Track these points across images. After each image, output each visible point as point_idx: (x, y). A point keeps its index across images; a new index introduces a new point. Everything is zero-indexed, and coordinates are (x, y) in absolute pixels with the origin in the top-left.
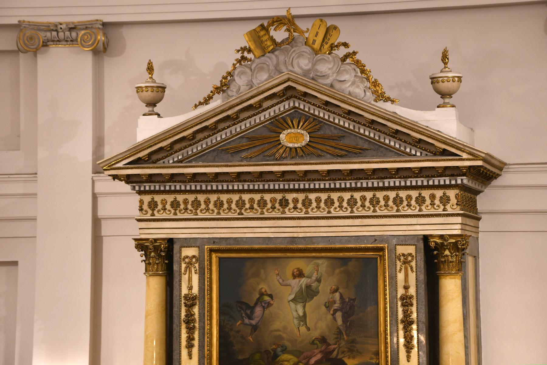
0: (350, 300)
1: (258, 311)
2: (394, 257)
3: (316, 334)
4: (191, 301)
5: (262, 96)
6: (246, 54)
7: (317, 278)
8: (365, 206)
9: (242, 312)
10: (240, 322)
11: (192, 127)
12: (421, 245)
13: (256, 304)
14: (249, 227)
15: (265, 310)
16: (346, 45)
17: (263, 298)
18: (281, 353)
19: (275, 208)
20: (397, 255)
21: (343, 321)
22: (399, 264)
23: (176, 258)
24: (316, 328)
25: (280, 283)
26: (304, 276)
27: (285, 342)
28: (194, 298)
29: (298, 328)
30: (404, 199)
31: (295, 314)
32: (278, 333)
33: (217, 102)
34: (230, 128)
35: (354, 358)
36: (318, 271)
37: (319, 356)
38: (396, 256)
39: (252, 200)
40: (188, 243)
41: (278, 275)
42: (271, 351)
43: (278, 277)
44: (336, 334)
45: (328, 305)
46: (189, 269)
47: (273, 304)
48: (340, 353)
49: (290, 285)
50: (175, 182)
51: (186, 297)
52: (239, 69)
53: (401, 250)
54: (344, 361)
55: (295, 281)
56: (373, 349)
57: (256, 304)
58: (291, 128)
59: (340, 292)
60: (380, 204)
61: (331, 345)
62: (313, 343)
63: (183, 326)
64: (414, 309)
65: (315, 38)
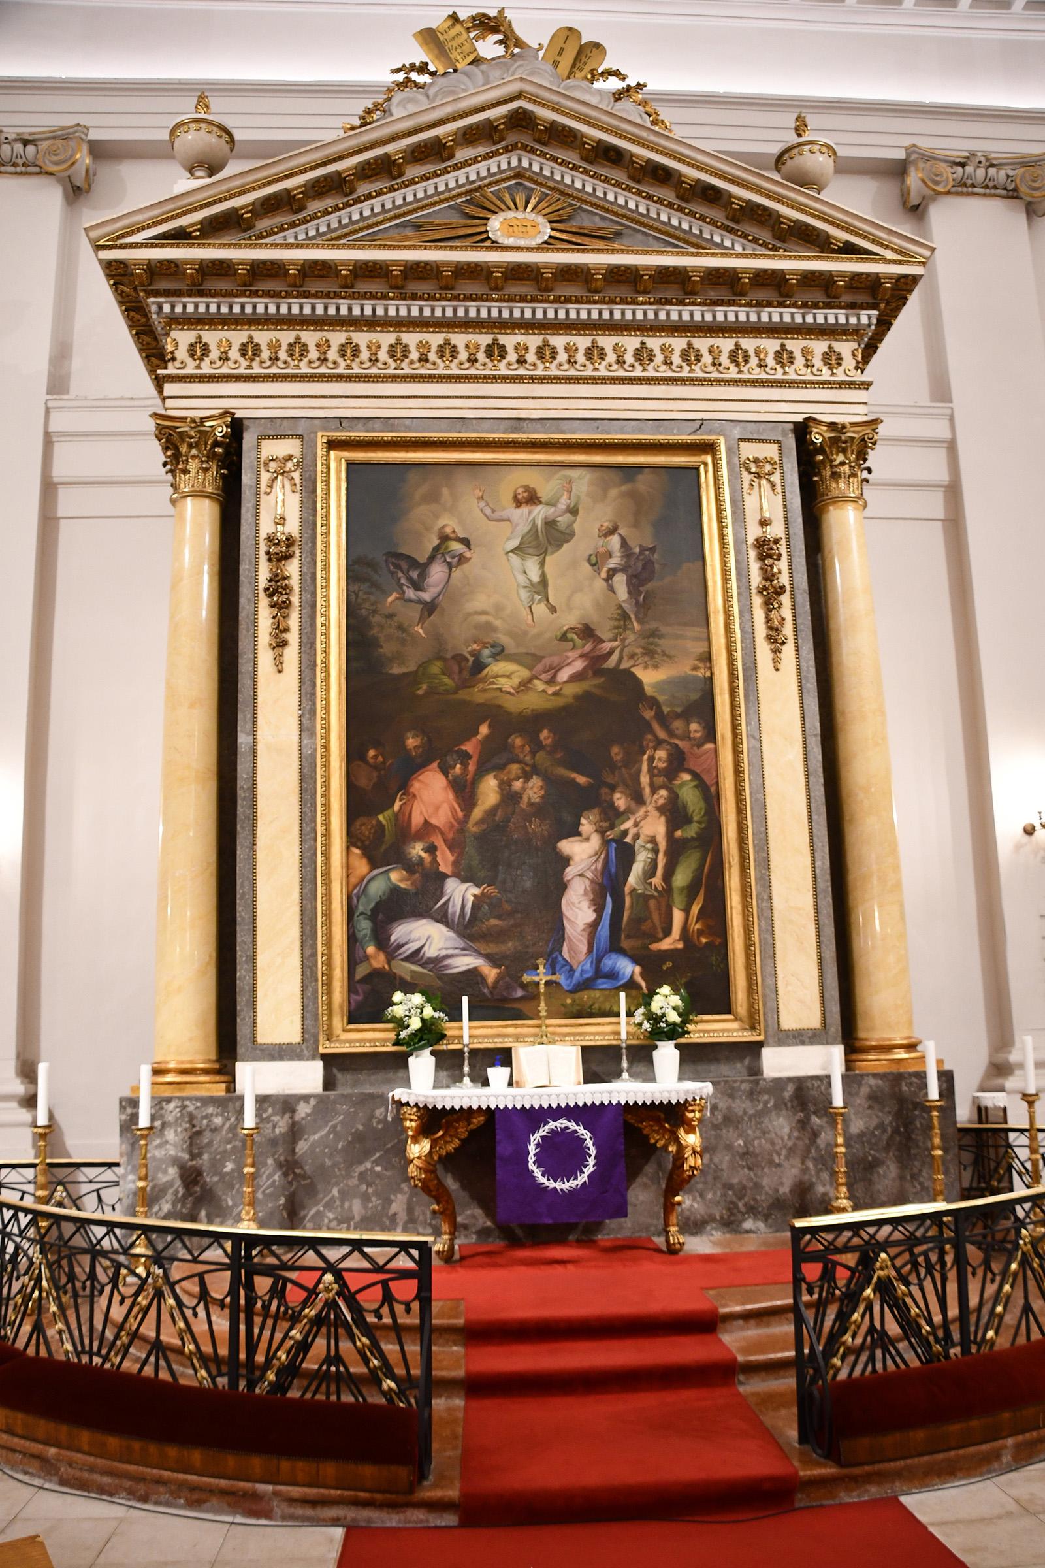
0: (643, 549)
1: (437, 572)
3: (570, 619)
4: (281, 552)
6: (414, 76)
7: (568, 506)
9: (400, 574)
10: (394, 595)
11: (305, 171)
12: (791, 442)
13: (432, 558)
16: (616, 74)
17: (447, 547)
18: (490, 659)
20: (742, 460)
21: (629, 592)
24: (569, 608)
25: (485, 515)
26: (541, 503)
27: (499, 635)
28: (290, 541)
31: (521, 579)
32: (483, 618)
34: (382, 198)
35: (656, 667)
36: (570, 492)
37: (579, 665)
39: (424, 346)
40: (276, 429)
41: (482, 498)
42: (468, 656)
43: (482, 504)
44: (616, 619)
45: (596, 561)
48: (625, 658)
50: (255, 294)
53: (749, 451)
54: (634, 675)
55: (519, 511)
56: (699, 648)
57: (432, 558)
58: (510, 209)
60: (703, 360)
62: (564, 638)
63: (264, 602)
64: (783, 565)
65: (558, 59)
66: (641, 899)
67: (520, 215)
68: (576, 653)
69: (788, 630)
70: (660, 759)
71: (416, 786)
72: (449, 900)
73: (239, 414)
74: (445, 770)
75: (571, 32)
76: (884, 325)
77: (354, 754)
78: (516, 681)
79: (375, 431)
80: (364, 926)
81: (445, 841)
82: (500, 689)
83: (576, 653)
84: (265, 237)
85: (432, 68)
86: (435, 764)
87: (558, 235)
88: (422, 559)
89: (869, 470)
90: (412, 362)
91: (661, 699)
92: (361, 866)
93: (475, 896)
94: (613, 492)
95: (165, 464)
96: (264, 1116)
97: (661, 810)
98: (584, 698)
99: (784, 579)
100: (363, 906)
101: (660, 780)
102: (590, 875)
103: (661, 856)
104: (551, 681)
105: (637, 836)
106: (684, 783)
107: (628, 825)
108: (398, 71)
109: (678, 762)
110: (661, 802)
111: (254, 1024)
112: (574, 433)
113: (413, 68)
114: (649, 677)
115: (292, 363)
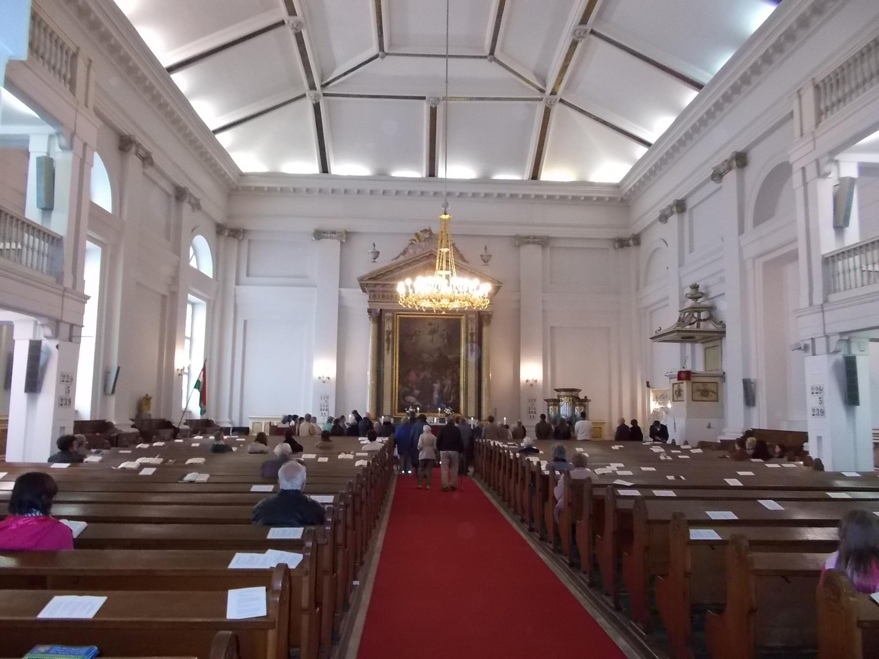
1: (414, 338)
5: (421, 257)
6: (413, 242)
12: (477, 314)
28: (390, 332)
33: (402, 258)
51: (387, 331)
52: (410, 247)
99: (474, 340)
114: (449, 357)
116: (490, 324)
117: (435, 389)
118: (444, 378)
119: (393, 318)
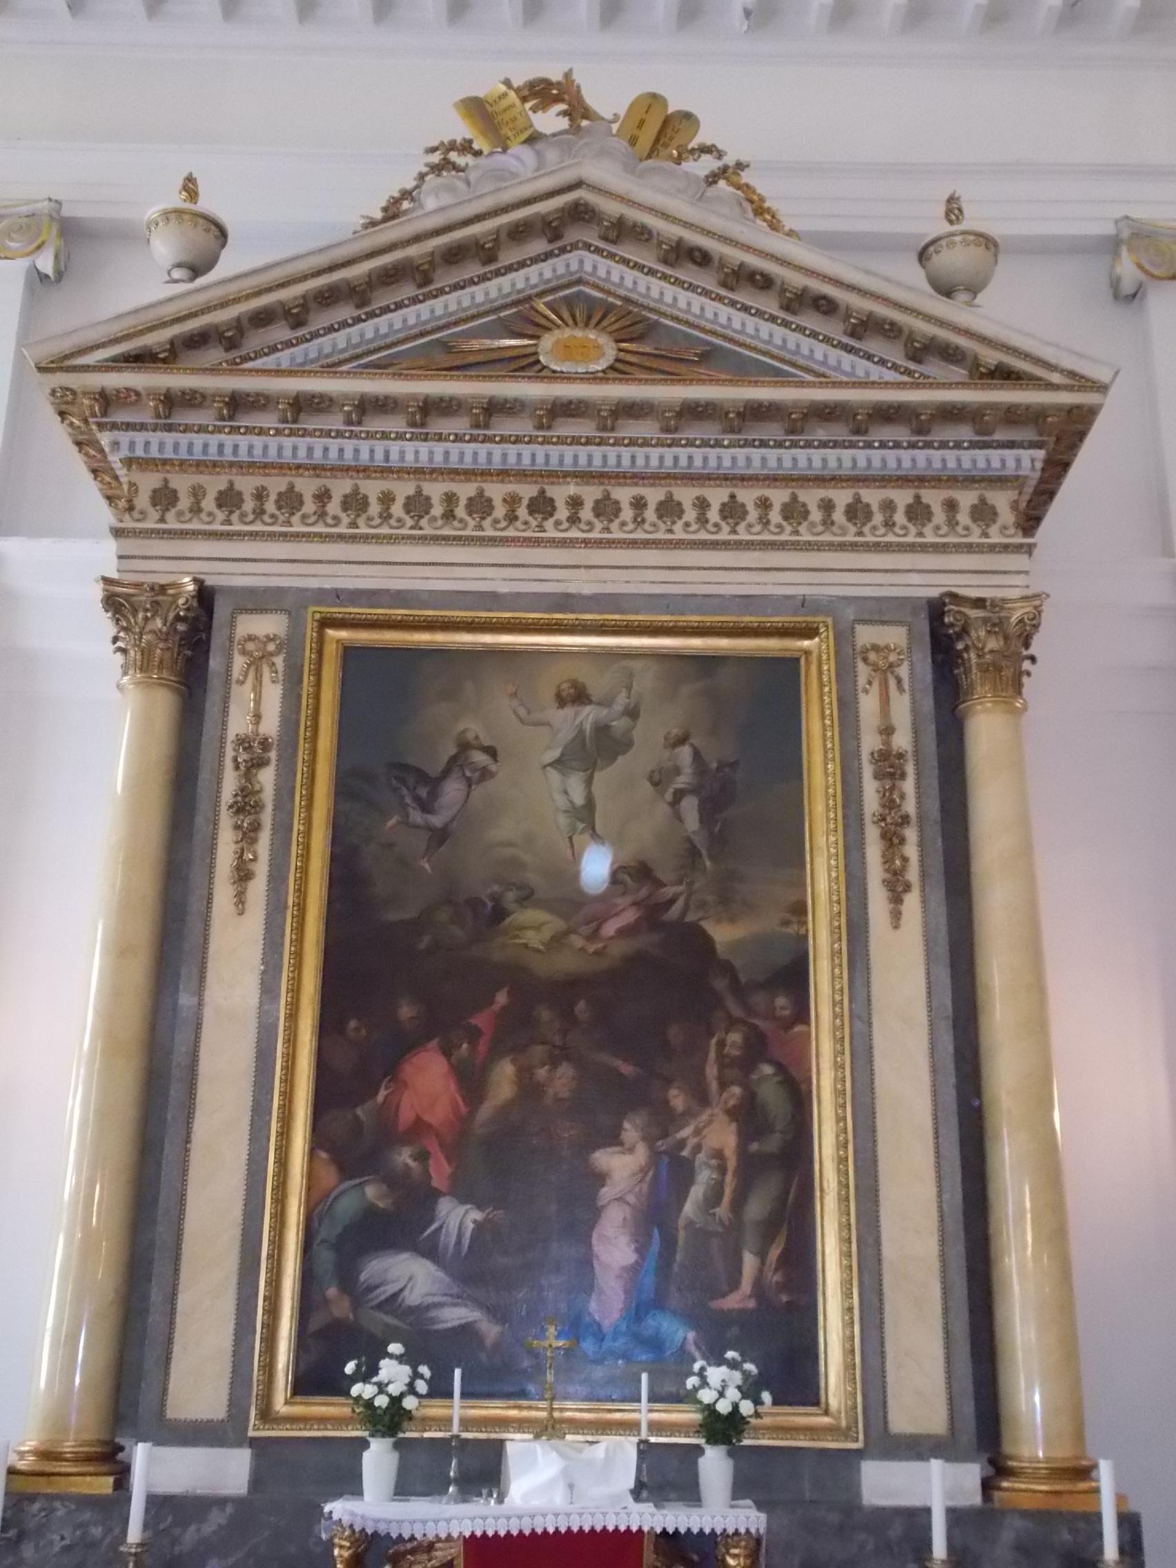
1: (452, 790)
2: (851, 651)
6: (453, 156)
8: (768, 522)
9: (405, 791)
12: (924, 626)
14: (440, 564)
15: (473, 787)
19: (516, 518)
21: (701, 821)
22: (863, 670)
23: (217, 640)
25: (518, 716)
28: (265, 744)
29: (570, 838)
30: (875, 508)
31: (561, 801)
32: (508, 852)
35: (732, 920)
36: (629, 688)
38: (854, 650)
41: (514, 695)
42: (487, 901)
43: (515, 703)
46: (257, 669)
47: (497, 772)
48: (692, 906)
49: (549, 724)
51: (244, 742)
55: (562, 712)
57: (446, 773)
59: (692, 745)
61: (665, 886)
63: (226, 821)
64: (909, 786)
66: (700, 1236)
67: (579, 333)
68: (629, 899)
69: (913, 875)
70: (733, 1045)
71: (408, 1070)
72: (441, 1227)
73: (210, 581)
74: (447, 1052)
75: (654, 100)
76: (1057, 467)
77: (327, 1027)
78: (547, 934)
79: (383, 607)
80: (325, 1258)
81: (441, 1146)
82: (526, 946)
83: (629, 899)
84: (251, 359)
85: (476, 146)
86: (434, 1043)
87: (629, 358)
88: (434, 770)
89: (1033, 659)
90: (434, 519)
91: (738, 963)
92: (328, 1175)
93: (475, 1222)
94: (686, 690)
95: (115, 639)
96: (162, 1527)
97: (732, 1114)
98: (636, 960)
99: (910, 807)
100: (327, 1232)
101: (733, 1073)
102: (631, 1199)
103: (729, 1178)
104: (594, 936)
105: (697, 1148)
106: (764, 1078)
107: (686, 1132)
108: (433, 150)
109: (757, 1049)
110: (732, 1102)
111: (165, 1391)
112: (637, 613)
113: (452, 146)
114: (723, 934)
115: (281, 518)
116: (1018, 688)
117: (607, 1193)
118: (678, 1099)
119: (290, 645)
